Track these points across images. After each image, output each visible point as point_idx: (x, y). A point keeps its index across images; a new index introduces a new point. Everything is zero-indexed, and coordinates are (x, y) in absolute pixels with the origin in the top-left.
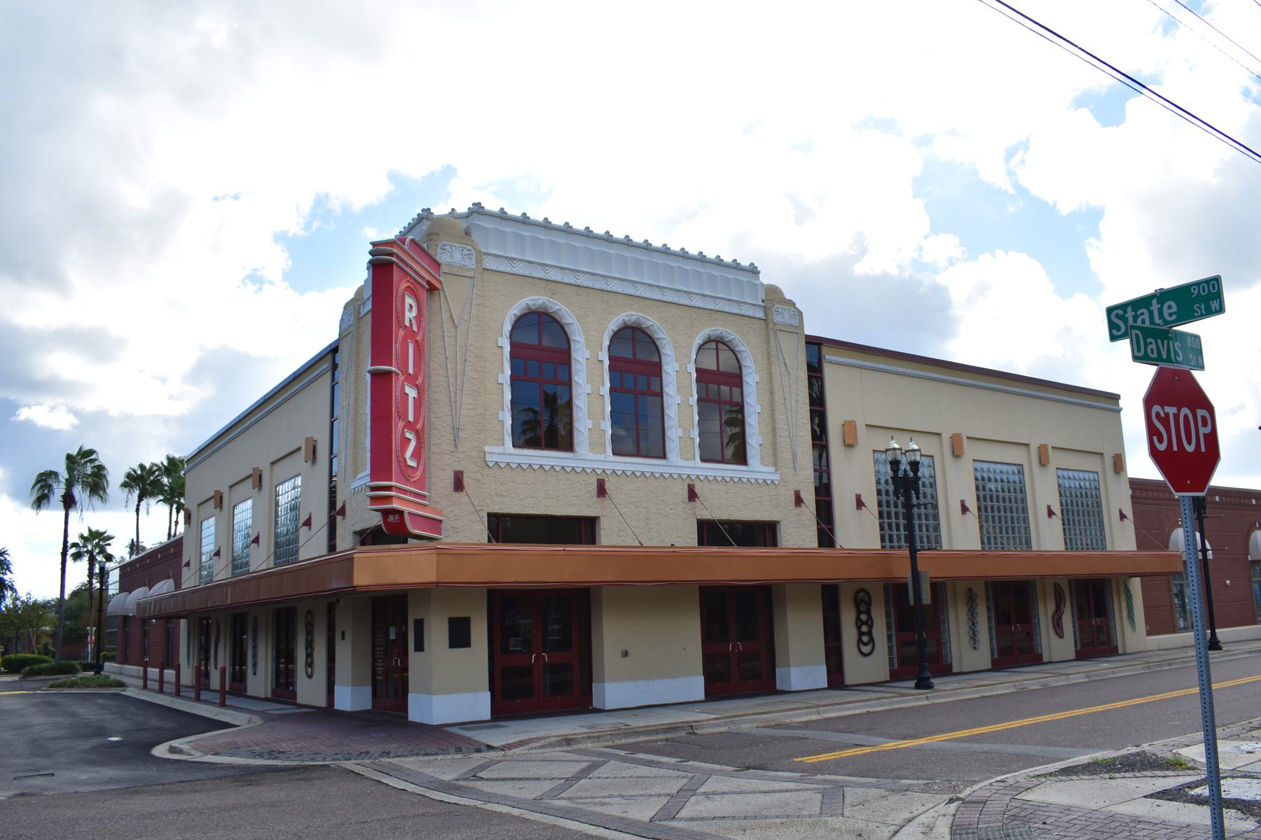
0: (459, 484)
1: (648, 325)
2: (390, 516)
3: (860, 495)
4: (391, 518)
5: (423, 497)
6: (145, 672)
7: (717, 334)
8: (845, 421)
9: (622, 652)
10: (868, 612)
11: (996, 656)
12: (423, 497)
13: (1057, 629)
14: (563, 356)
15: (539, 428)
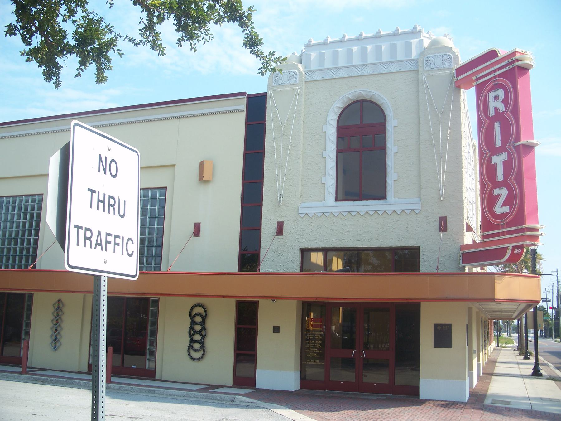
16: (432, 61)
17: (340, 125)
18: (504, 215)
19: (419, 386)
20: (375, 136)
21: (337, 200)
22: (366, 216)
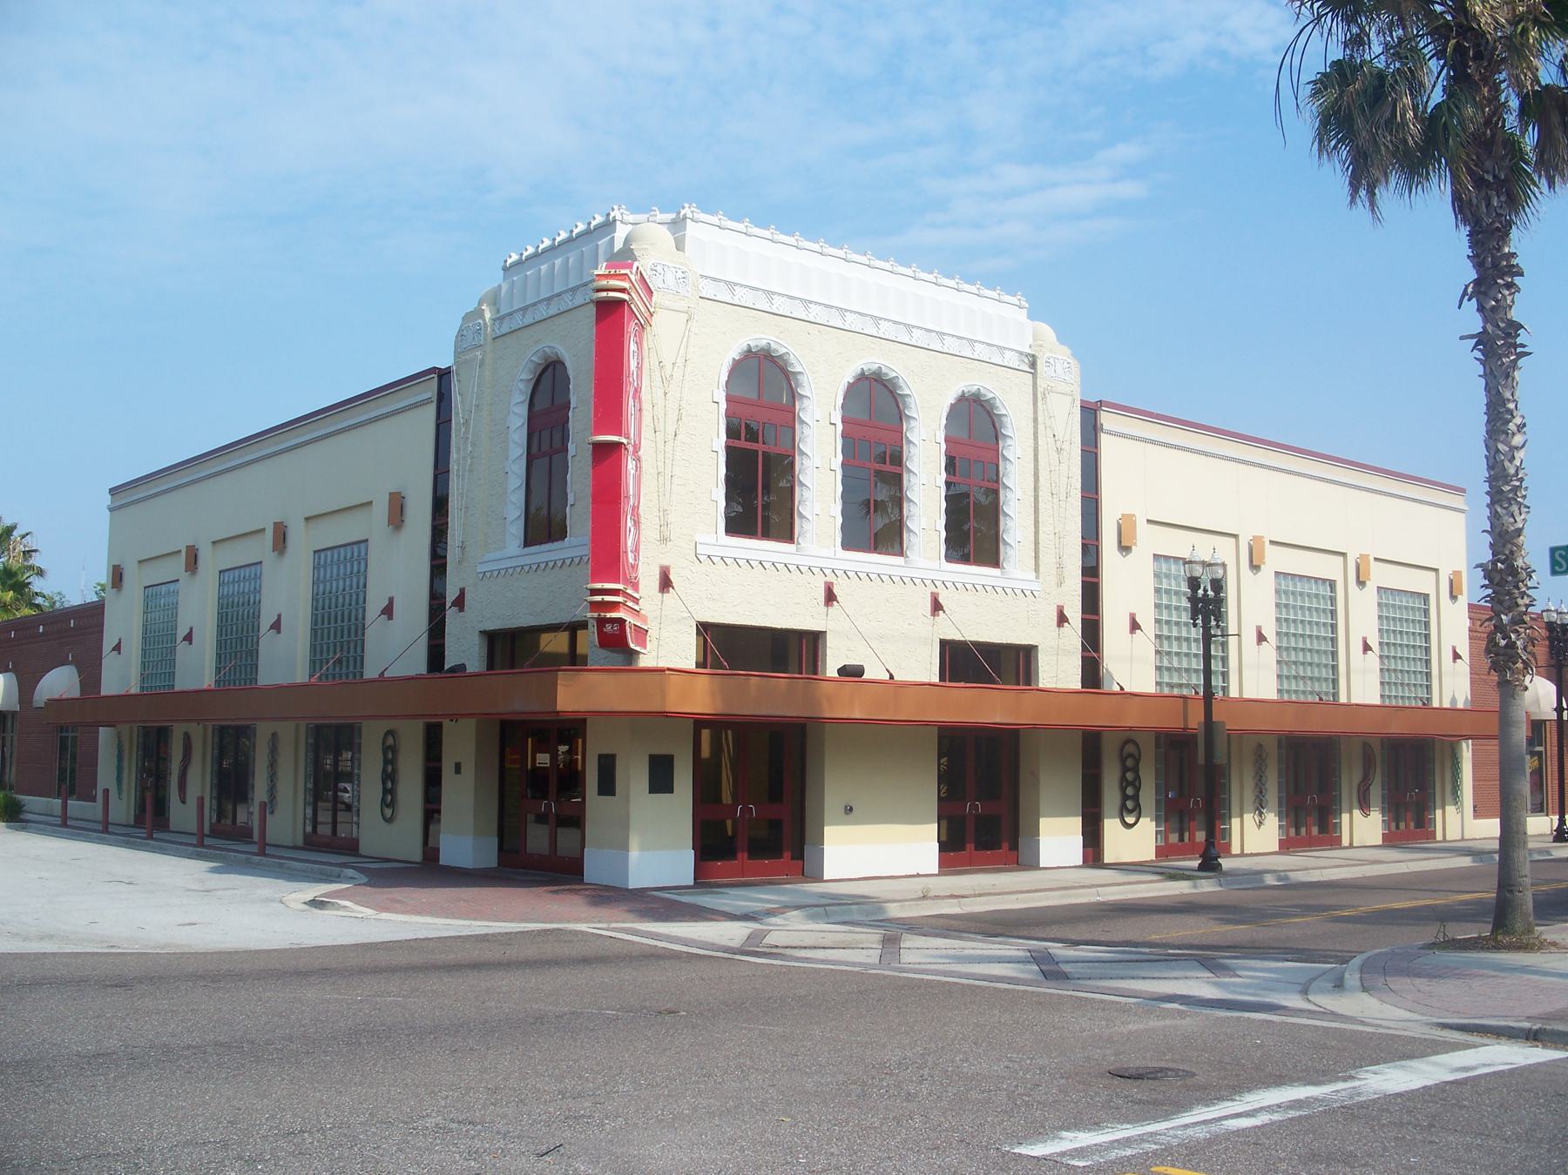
0: (666, 583)
1: (891, 376)
2: (607, 625)
4: (608, 628)
6: (65, 807)
8: (1123, 515)
9: (846, 807)
10: (1135, 770)
11: (137, 812)
13: (1362, 803)
14: (787, 417)
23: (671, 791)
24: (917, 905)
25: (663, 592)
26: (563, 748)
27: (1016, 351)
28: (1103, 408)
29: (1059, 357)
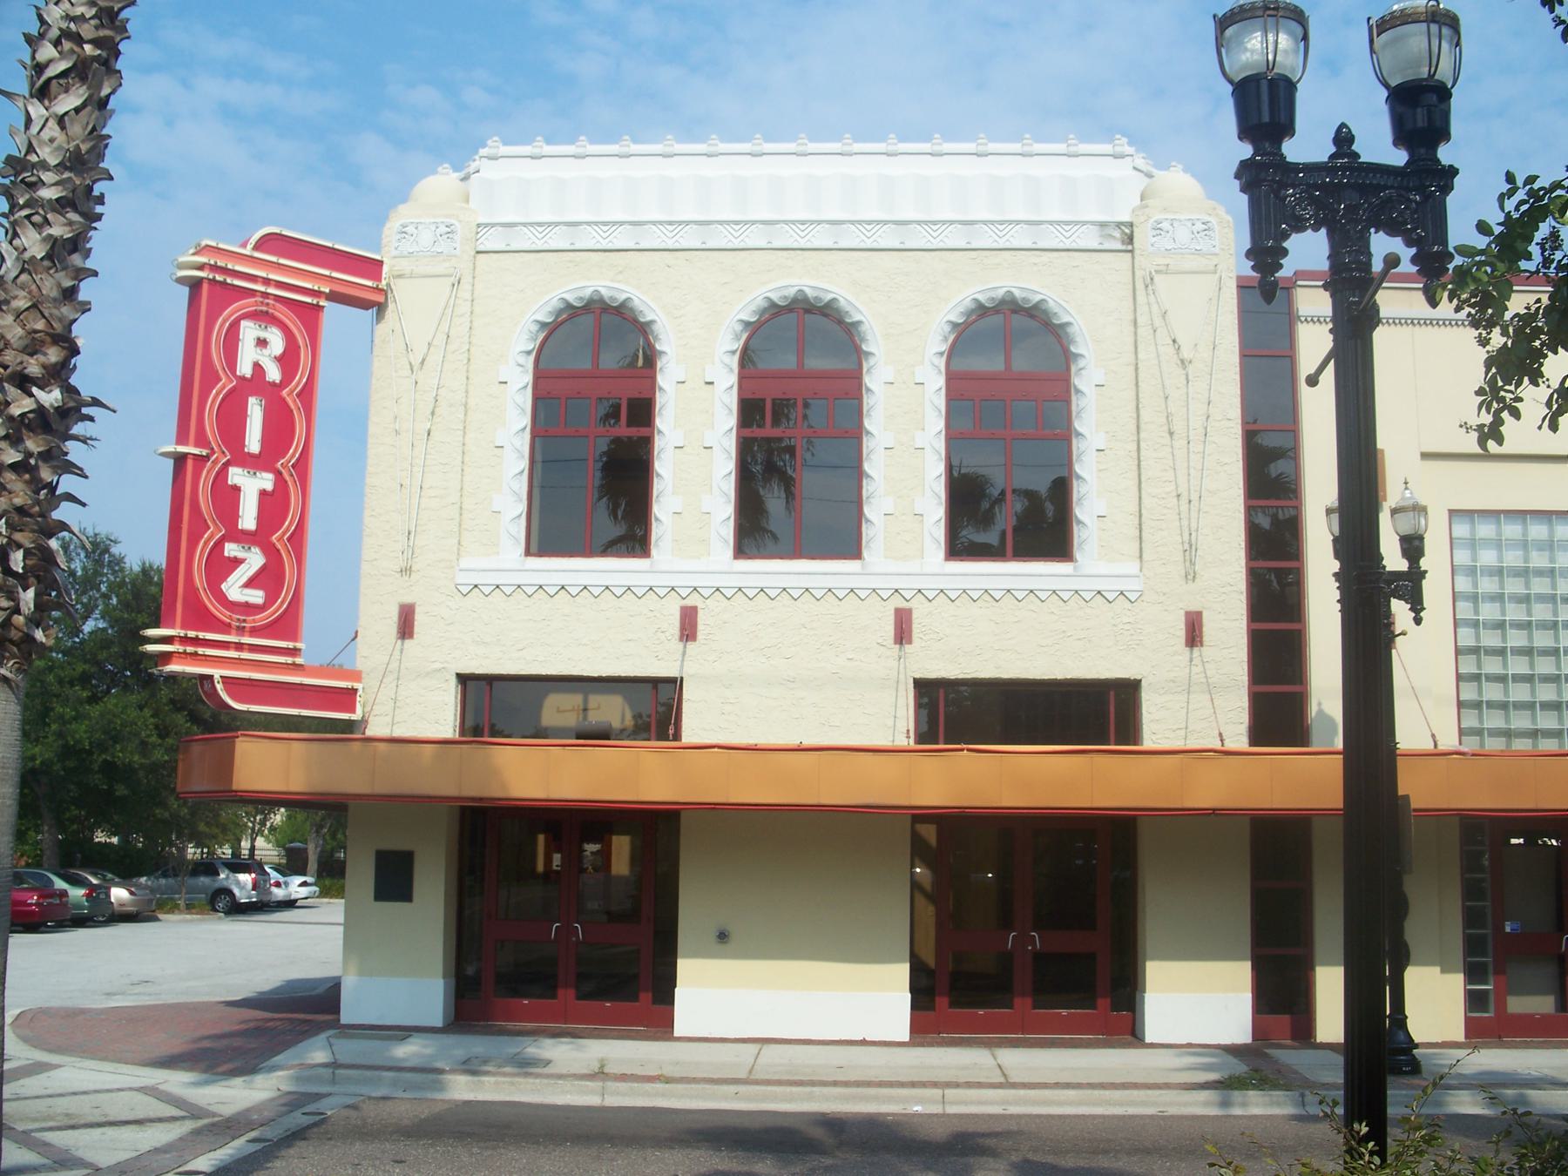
0: (406, 626)
3: (1199, 614)
5: (294, 652)
7: (1000, 297)
12: (294, 652)
15: (765, 521)
16: (1168, 232)
17: (541, 366)
18: (248, 608)
19: (911, 1033)
20: (836, 402)
21: (528, 553)
22: (519, 595)
23: (407, 897)
24: (512, 1084)
25: (901, 643)
26: (591, 848)
27: (1093, 223)
28: (1299, 283)
29: (1182, 217)
